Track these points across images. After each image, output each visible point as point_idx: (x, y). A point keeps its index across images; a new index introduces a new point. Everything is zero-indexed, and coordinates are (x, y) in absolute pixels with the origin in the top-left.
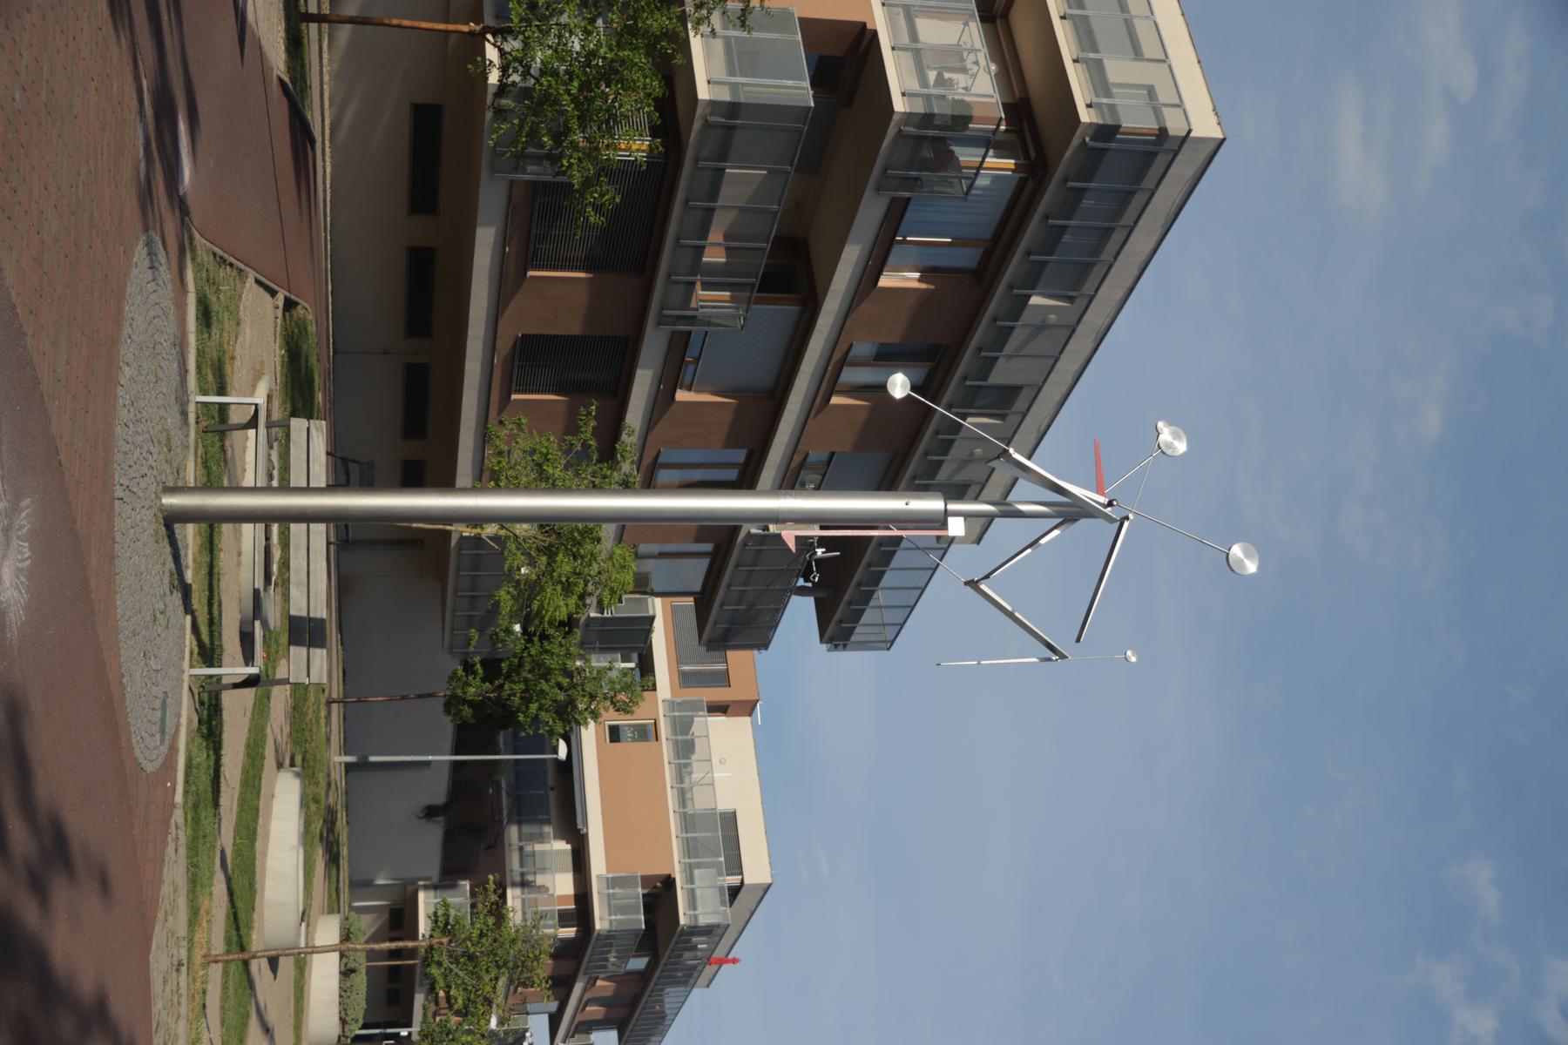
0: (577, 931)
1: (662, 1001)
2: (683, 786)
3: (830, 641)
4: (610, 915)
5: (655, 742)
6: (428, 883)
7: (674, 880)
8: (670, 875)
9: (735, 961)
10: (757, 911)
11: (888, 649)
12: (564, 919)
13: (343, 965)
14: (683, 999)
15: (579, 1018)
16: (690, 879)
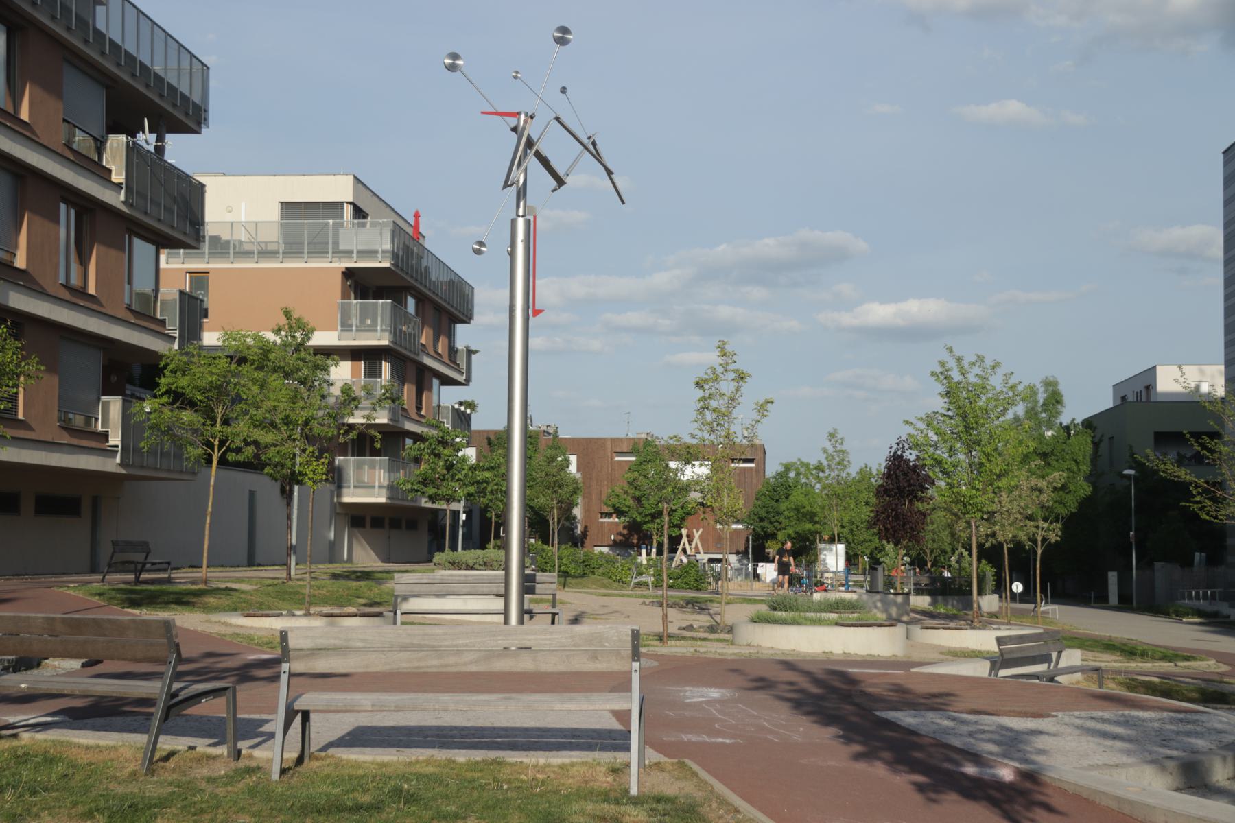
0: (385, 361)
1: (442, 282)
2: (256, 252)
3: (199, 124)
4: (376, 331)
5: (209, 275)
6: (335, 493)
7: (347, 268)
8: (343, 273)
9: (417, 216)
10: (373, 190)
11: (208, 68)
12: (373, 372)
13: (481, 568)
14: (445, 268)
15: (446, 360)
16: (348, 253)
